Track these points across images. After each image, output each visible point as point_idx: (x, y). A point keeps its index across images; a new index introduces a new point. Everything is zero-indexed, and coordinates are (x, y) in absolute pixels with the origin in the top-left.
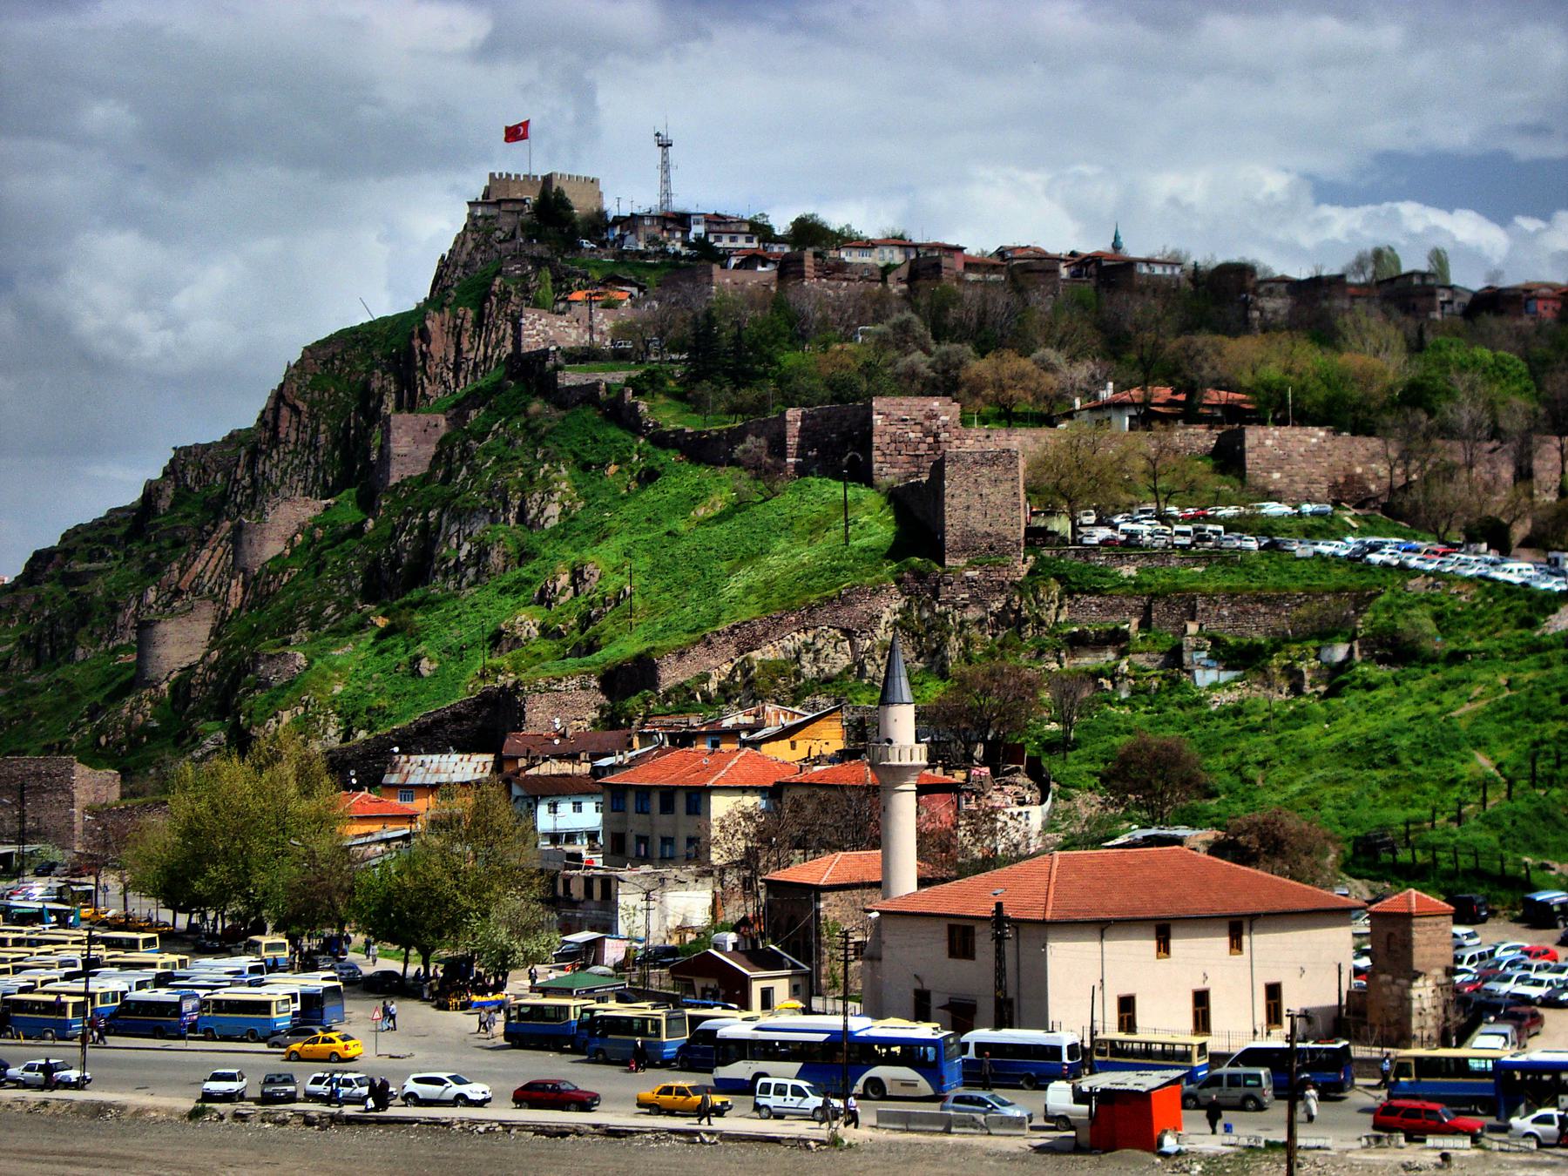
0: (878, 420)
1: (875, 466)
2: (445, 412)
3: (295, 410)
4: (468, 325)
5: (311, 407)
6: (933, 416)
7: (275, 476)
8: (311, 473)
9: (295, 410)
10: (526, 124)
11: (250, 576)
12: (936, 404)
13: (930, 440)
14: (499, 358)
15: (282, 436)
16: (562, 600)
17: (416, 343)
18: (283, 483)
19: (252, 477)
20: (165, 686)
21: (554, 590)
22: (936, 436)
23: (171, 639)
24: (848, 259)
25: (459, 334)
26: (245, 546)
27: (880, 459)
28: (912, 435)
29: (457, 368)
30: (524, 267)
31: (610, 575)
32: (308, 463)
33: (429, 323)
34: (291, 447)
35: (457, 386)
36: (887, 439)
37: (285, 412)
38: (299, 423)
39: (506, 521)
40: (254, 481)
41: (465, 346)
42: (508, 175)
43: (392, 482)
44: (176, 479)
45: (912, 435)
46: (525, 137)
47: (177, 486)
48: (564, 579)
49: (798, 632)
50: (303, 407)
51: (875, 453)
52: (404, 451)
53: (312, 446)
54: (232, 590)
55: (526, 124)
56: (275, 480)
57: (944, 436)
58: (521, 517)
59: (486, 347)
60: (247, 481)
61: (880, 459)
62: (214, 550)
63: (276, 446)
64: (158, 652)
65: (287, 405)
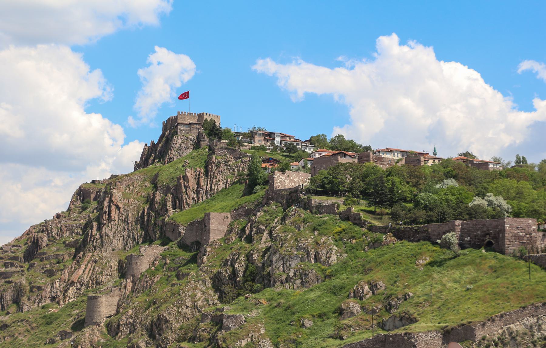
0: (507, 226)
1: (506, 246)
2: (230, 213)
3: (118, 207)
4: (202, 175)
5: (124, 205)
6: (529, 225)
7: (110, 234)
8: (126, 234)
9: (118, 207)
10: (188, 93)
11: (136, 279)
12: (530, 221)
13: (528, 236)
14: (218, 189)
15: (113, 217)
16: (368, 296)
17: (182, 181)
18: (114, 237)
19: (100, 235)
20: (102, 324)
21: (363, 292)
22: (530, 234)
23: (104, 304)
24: (383, 156)
25: (199, 178)
26: (134, 266)
27: (508, 243)
28: (521, 234)
29: (198, 193)
30: (224, 152)
31: (510, 289)
32: (125, 229)
33: (187, 173)
34: (116, 222)
35: (198, 200)
36: (511, 235)
37: (113, 207)
38: (119, 213)
39: (309, 261)
40: (101, 237)
41: (202, 183)
42: (185, 113)
43: (210, 240)
44: (48, 234)
45: (521, 234)
46: (188, 97)
47: (49, 237)
48: (367, 288)
49: (530, 317)
50: (121, 206)
51: (506, 240)
52: (216, 228)
53: (126, 222)
54: (128, 284)
55: (188, 93)
56: (111, 236)
57: (533, 234)
58: (317, 259)
59: (211, 185)
60: (98, 236)
61: (508, 243)
62: (86, 265)
63: (110, 222)
64: (99, 309)
65: (114, 204)
